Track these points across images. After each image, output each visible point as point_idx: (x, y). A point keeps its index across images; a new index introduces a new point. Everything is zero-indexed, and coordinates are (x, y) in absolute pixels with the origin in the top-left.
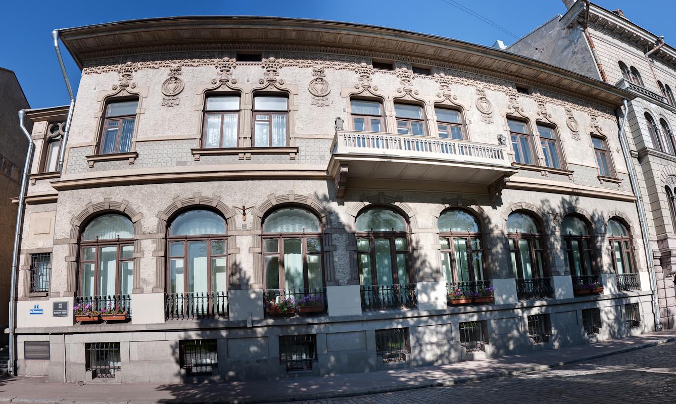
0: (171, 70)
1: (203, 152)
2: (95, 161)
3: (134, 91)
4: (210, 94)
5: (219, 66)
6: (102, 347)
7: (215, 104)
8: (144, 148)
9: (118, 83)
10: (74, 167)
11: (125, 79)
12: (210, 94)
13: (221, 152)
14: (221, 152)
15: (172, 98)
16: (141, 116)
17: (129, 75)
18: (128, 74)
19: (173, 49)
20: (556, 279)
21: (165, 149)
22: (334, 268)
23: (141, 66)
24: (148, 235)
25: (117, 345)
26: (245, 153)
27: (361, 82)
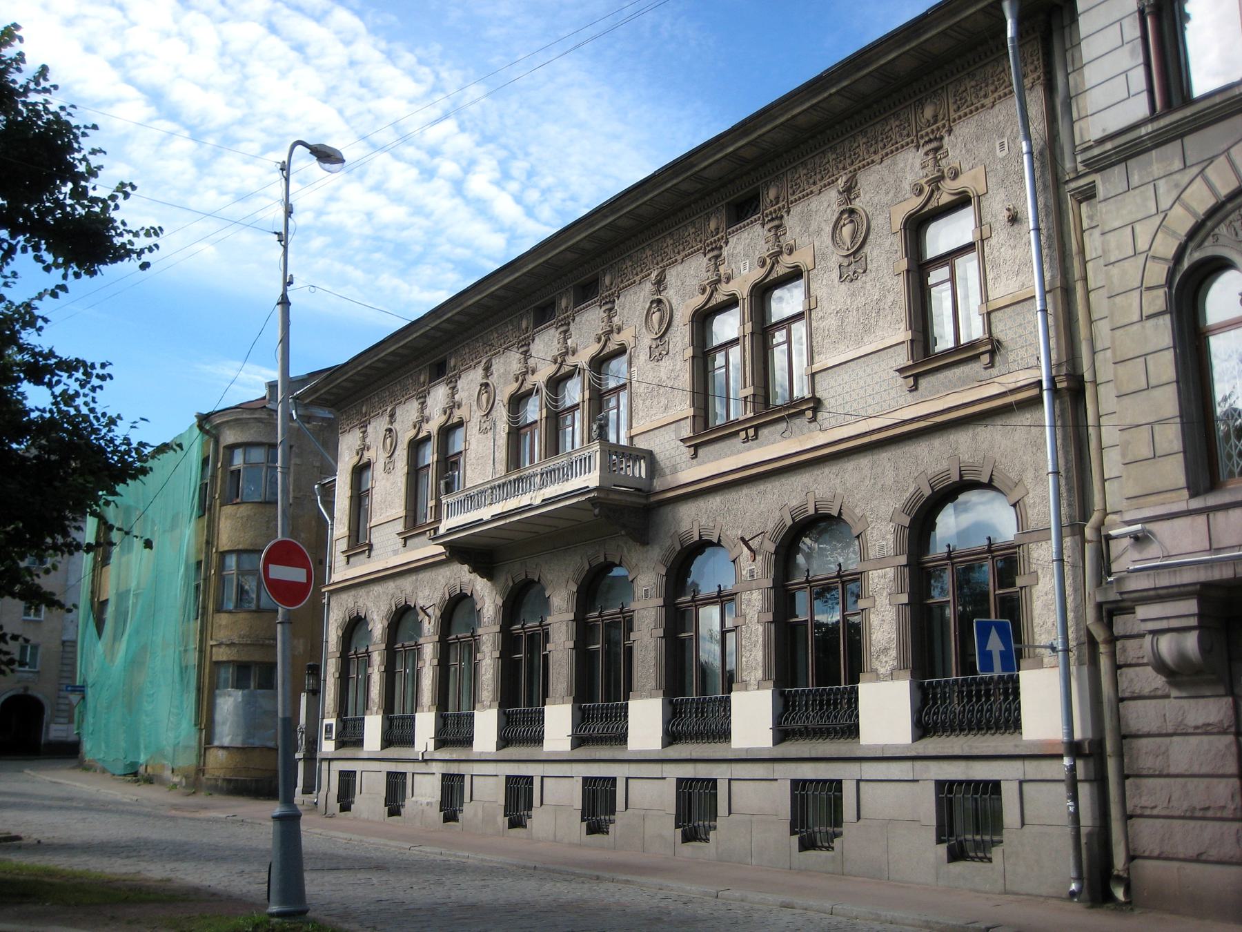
24: (880, 562)
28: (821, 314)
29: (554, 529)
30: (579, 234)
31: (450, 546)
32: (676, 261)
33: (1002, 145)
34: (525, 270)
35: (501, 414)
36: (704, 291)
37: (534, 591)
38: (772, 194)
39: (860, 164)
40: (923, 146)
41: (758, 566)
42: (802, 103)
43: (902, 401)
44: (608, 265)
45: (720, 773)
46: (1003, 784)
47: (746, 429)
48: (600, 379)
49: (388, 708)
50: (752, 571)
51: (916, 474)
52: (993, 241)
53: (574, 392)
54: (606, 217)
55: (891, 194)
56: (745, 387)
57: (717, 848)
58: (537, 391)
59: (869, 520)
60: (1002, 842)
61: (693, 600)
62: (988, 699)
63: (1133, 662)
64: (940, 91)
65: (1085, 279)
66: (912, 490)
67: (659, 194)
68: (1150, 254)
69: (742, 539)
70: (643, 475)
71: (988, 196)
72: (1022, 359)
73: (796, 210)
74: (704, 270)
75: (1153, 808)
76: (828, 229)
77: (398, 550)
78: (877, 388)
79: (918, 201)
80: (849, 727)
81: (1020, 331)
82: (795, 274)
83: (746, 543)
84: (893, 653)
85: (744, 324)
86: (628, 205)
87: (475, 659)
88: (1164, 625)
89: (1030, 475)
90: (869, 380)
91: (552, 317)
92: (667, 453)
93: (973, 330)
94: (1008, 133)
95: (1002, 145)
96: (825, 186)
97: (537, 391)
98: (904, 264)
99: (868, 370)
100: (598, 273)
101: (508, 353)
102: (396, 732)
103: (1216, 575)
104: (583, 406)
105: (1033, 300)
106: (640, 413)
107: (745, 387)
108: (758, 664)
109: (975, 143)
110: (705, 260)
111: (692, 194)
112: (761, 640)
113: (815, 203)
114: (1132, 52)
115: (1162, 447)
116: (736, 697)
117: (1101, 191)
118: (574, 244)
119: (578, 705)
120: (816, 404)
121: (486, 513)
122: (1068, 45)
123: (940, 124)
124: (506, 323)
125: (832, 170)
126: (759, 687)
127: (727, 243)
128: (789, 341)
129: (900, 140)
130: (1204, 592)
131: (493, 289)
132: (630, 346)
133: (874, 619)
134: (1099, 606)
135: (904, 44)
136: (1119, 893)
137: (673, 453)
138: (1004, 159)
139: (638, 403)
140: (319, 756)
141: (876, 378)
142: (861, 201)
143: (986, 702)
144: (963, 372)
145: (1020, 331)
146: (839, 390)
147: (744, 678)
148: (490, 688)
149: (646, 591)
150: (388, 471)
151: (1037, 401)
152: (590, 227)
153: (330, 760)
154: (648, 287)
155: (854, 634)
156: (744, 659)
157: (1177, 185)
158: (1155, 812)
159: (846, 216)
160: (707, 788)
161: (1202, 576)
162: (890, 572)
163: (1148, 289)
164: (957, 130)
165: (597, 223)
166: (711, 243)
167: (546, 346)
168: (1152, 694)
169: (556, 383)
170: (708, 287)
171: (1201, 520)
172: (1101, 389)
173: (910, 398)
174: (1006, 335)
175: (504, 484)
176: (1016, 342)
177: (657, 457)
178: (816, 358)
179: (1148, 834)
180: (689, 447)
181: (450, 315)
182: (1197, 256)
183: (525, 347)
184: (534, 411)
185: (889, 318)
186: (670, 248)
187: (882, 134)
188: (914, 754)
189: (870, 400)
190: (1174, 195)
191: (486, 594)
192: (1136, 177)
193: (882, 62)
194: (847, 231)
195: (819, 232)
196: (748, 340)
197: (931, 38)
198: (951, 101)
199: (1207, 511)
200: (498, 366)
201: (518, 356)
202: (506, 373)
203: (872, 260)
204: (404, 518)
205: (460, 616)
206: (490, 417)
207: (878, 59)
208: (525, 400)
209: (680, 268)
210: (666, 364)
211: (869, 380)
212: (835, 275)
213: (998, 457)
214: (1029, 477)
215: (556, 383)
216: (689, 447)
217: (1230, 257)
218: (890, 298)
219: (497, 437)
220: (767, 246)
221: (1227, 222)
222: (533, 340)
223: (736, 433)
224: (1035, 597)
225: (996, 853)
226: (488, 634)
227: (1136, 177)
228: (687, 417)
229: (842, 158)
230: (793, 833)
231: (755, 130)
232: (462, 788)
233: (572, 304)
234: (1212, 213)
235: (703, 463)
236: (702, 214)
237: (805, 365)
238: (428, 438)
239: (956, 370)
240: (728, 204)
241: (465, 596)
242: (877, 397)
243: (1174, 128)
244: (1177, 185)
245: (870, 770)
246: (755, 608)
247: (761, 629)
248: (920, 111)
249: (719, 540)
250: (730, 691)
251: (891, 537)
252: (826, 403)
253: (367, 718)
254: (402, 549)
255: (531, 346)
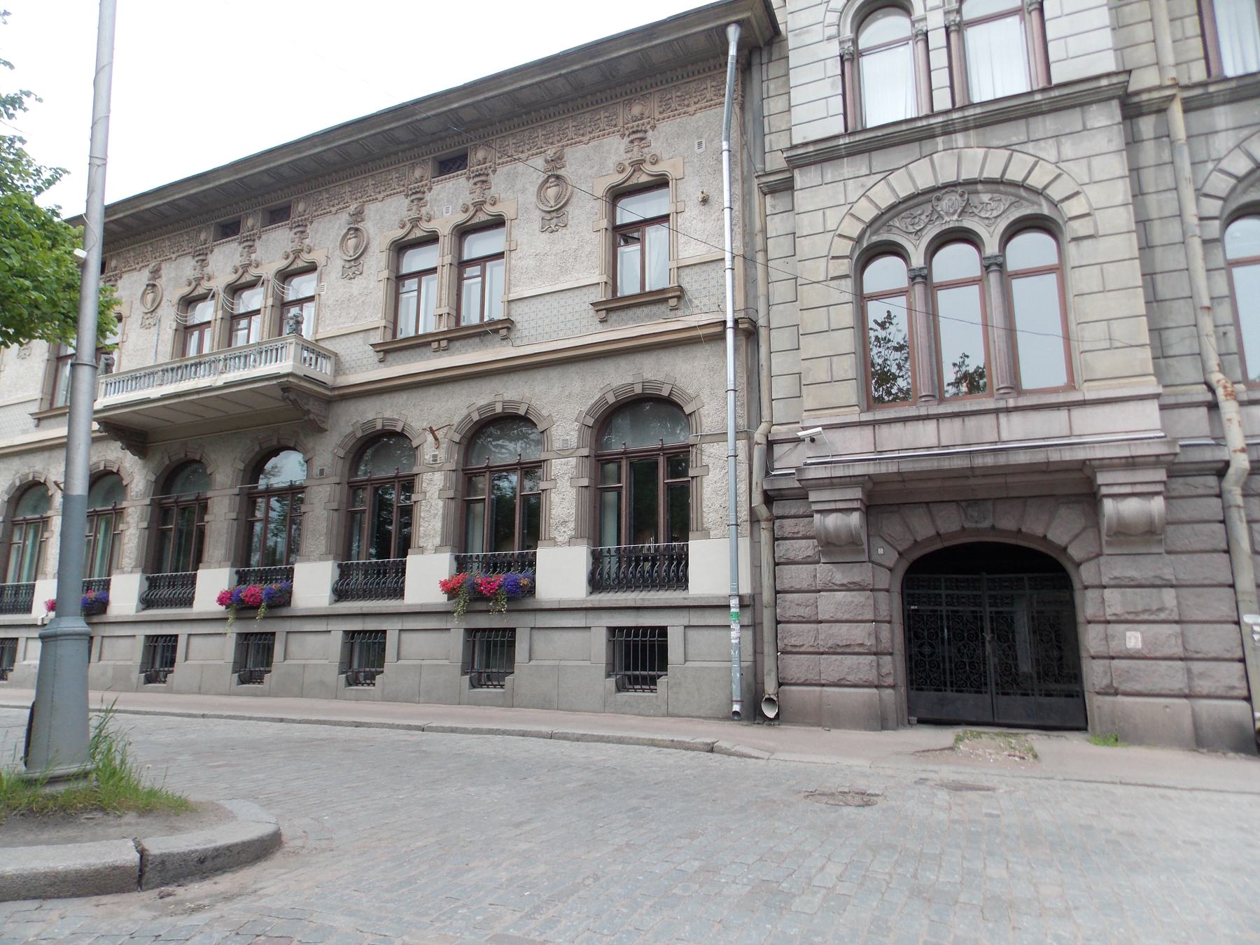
0: (547, 161)
1: (390, 349)
2: (608, 310)
3: (494, 210)
4: (618, 194)
5: (627, 133)
6: (644, 635)
7: (631, 211)
8: (566, 302)
9: (626, 159)
10: (370, 362)
11: (636, 149)
12: (618, 194)
13: (420, 343)
14: (420, 343)
15: (555, 216)
16: (513, 253)
17: (642, 139)
18: (638, 136)
19: (541, 118)
20: (696, 547)
21: (713, 278)
22: (702, 515)
23: (661, 116)
24: (563, 453)
25: (663, 631)
26: (439, 341)
27: (629, 155)
28: (520, 255)
29: (169, 424)
30: (284, 158)
31: (105, 422)
32: (331, 212)
33: (700, 144)
34: (217, 183)
36: (190, 284)
38: (301, 207)
39: (597, 134)
40: (629, 136)
41: (442, 454)
42: (533, 77)
43: (592, 330)
44: (304, 194)
46: (518, 631)
47: (439, 341)
48: (232, 304)
50: (435, 457)
51: (602, 386)
52: (686, 215)
54: (315, 146)
55: (596, 168)
56: (440, 307)
57: (383, 690)
58: (213, 296)
59: (555, 419)
60: (382, 672)
61: (114, 509)
62: (384, 576)
63: (789, 536)
64: (648, 96)
65: (766, 251)
66: (597, 397)
67: (373, 135)
68: (838, 232)
69: (431, 428)
70: (328, 372)
71: (684, 180)
72: (705, 305)
73: (502, 170)
74: (405, 209)
75: (803, 645)
76: (140, 294)
77: (28, 429)
78: (569, 317)
79: (234, 277)
80: (395, 590)
81: (704, 284)
82: (311, 268)
83: (432, 431)
84: (572, 525)
85: (443, 256)
86: (340, 139)
87: (42, 537)
88: (832, 506)
89: (707, 391)
90: (562, 311)
91: (462, 167)
92: (354, 356)
93: (496, 312)
94: (706, 135)
95: (700, 144)
96: (387, 196)
97: (213, 296)
98: (385, 274)
99: (562, 303)
100: (291, 201)
101: (181, 260)
104: (265, 311)
105: (721, 264)
106: (327, 322)
107: (440, 307)
108: (436, 532)
109: (676, 140)
110: (408, 201)
111: (402, 143)
112: (441, 512)
113: (135, 275)
114: (833, 85)
115: (839, 374)
116: (412, 561)
117: (799, 182)
118: (275, 167)
119: (235, 569)
120: (680, 294)
121: (155, 392)
122: (765, 78)
123: (488, 165)
124: (129, 250)
125: (347, 199)
126: (437, 550)
127: (430, 189)
128: (249, 328)
129: (397, 187)
131: (177, 196)
133: (555, 497)
134: (765, 492)
135: (636, 44)
136: (770, 713)
137: (360, 356)
138: (700, 155)
139: (326, 313)
141: (569, 309)
142: (566, 171)
143: (396, 576)
144: (651, 311)
145: (704, 284)
146: (533, 316)
147: (421, 545)
148: (133, 555)
149: (322, 471)
151: (721, 337)
152: (296, 153)
154: (344, 217)
155: (533, 511)
156: (421, 529)
157: (863, 186)
158: (802, 649)
159: (352, 232)
160: (170, 641)
161: (871, 469)
162: (573, 461)
163: (833, 258)
164: (660, 126)
165: (304, 151)
166: (247, 236)
168: (804, 560)
170: (291, 254)
171: (868, 431)
172: (773, 333)
173: (600, 327)
174: (692, 286)
175: (179, 368)
176: (701, 293)
177: (342, 360)
178: (513, 289)
179: (796, 666)
180: (377, 352)
181: (121, 215)
182: (875, 239)
183: (202, 256)
185: (585, 264)
186: (186, 242)
187: (529, 139)
188: (589, 605)
189: (562, 326)
190: (861, 192)
191: (136, 471)
192: (829, 175)
193: (615, 55)
194: (352, 243)
195: (524, 191)
196: (268, 311)
197: (696, 33)
198: (656, 106)
199: (874, 423)
200: (168, 271)
201: (193, 263)
203: (573, 218)
204: (39, 400)
205: (29, 499)
206: (154, 314)
207: (611, 52)
208: (195, 303)
209: (379, 204)
210: (358, 285)
211: (562, 311)
212: (537, 225)
213: (678, 376)
214: (705, 396)
216: (377, 352)
217: (970, 227)
218: (588, 249)
219: (161, 333)
220: (240, 259)
221: (900, 217)
222: (212, 251)
223: (429, 344)
224: (705, 485)
225: (662, 682)
226: (135, 506)
227: (829, 175)
228: (378, 328)
229: (583, 126)
230: (464, 673)
231: (483, 93)
233: (211, 238)
234: (892, 207)
235: (391, 365)
236: (408, 163)
237: (311, 333)
239: (644, 309)
240: (434, 158)
242: (569, 325)
243: (867, 143)
244: (863, 186)
246: (436, 487)
247: (441, 503)
248: (473, 153)
249: (118, 471)
250: (405, 555)
251: (575, 434)
252: (519, 326)
254: (34, 429)
255: (209, 256)
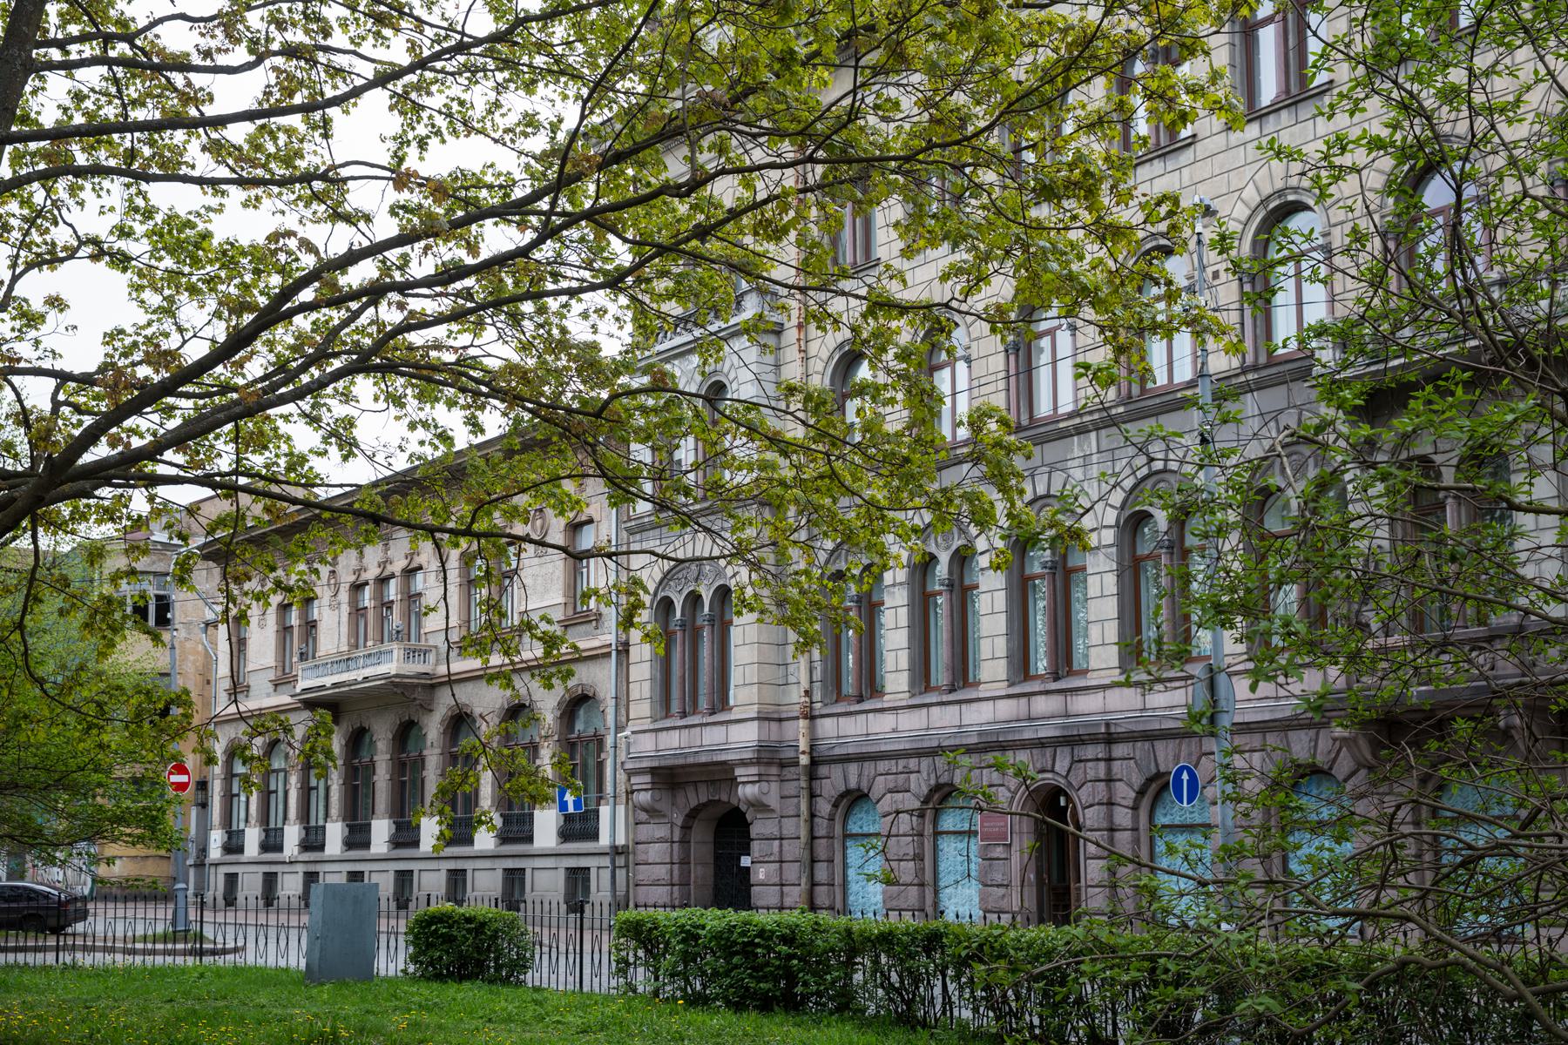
35: (344, 596)
37: (414, 732)
45: (468, 865)
49: (304, 815)
53: (393, 591)
102: (272, 840)
103: (664, 763)
130: (653, 771)
132: (425, 565)
140: (207, 861)
150: (262, 626)
151: (608, 655)
153: (216, 865)
161: (655, 764)
167: (373, 554)
169: (383, 581)
184: (367, 598)
202: (348, 566)
215: (383, 581)
232: (465, 881)
238: (392, 576)
241: (524, 706)
245: (539, 863)
253: (374, 823)
